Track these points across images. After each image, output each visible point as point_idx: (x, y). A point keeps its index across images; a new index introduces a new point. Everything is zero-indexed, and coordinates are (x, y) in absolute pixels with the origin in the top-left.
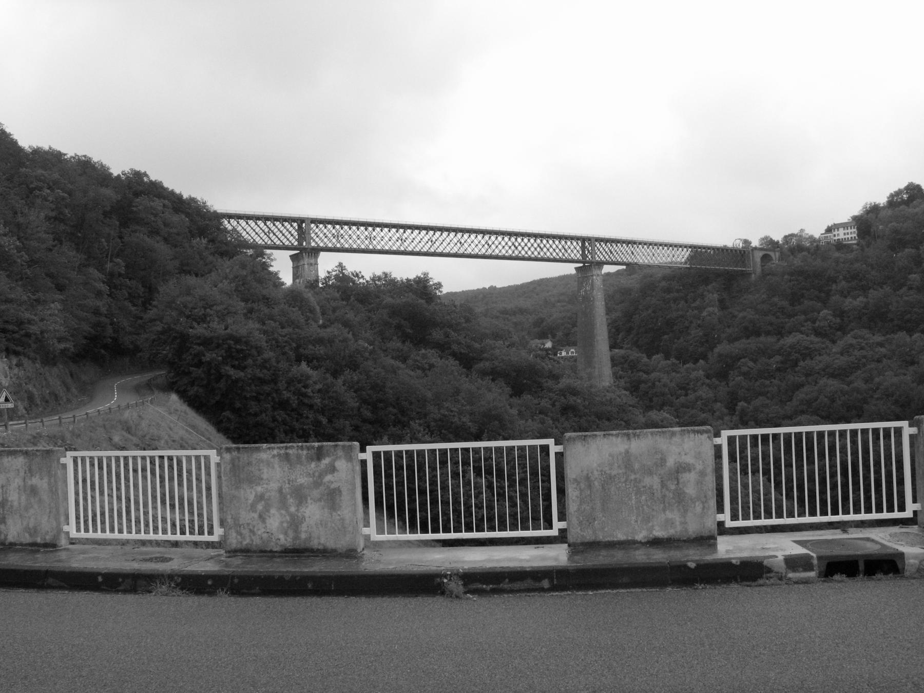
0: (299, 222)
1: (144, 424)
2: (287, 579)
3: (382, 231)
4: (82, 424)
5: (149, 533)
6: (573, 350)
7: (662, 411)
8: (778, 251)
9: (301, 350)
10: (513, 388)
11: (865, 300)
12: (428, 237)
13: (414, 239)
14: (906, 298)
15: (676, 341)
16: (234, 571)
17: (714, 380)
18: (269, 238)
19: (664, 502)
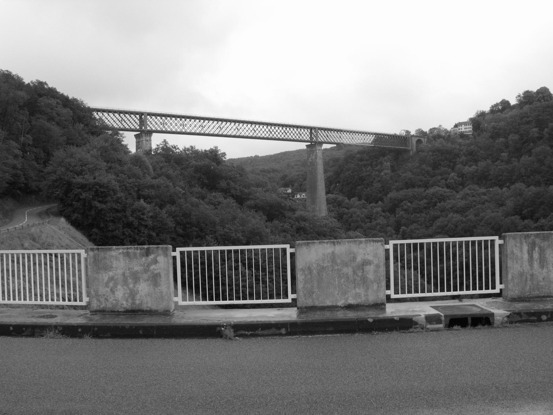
0: (140, 115)
1: (43, 236)
2: (127, 328)
3: (190, 121)
4: (5, 236)
5: (60, 301)
6: (304, 194)
7: (356, 231)
8: (426, 138)
9: (140, 192)
10: (267, 216)
11: (476, 167)
12: (223, 130)
13: (209, 126)
14: (500, 167)
15: (365, 189)
16: (94, 324)
17: (387, 213)
18: (122, 124)
19: (355, 283)
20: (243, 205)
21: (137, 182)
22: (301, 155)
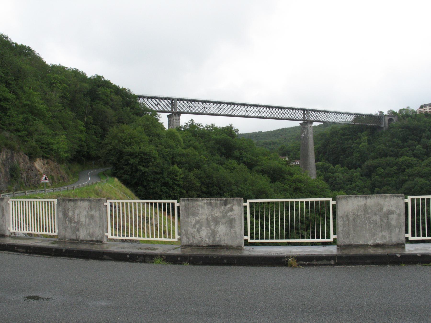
0: (172, 100)
1: (104, 191)
10: (271, 179)
13: (225, 108)
15: (347, 158)
17: (364, 177)
18: (158, 107)
20: (253, 170)
21: (172, 151)
22: (295, 131)
